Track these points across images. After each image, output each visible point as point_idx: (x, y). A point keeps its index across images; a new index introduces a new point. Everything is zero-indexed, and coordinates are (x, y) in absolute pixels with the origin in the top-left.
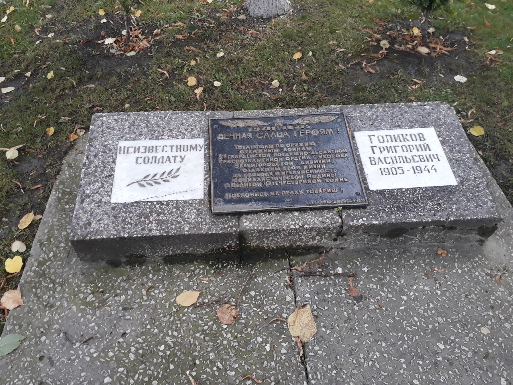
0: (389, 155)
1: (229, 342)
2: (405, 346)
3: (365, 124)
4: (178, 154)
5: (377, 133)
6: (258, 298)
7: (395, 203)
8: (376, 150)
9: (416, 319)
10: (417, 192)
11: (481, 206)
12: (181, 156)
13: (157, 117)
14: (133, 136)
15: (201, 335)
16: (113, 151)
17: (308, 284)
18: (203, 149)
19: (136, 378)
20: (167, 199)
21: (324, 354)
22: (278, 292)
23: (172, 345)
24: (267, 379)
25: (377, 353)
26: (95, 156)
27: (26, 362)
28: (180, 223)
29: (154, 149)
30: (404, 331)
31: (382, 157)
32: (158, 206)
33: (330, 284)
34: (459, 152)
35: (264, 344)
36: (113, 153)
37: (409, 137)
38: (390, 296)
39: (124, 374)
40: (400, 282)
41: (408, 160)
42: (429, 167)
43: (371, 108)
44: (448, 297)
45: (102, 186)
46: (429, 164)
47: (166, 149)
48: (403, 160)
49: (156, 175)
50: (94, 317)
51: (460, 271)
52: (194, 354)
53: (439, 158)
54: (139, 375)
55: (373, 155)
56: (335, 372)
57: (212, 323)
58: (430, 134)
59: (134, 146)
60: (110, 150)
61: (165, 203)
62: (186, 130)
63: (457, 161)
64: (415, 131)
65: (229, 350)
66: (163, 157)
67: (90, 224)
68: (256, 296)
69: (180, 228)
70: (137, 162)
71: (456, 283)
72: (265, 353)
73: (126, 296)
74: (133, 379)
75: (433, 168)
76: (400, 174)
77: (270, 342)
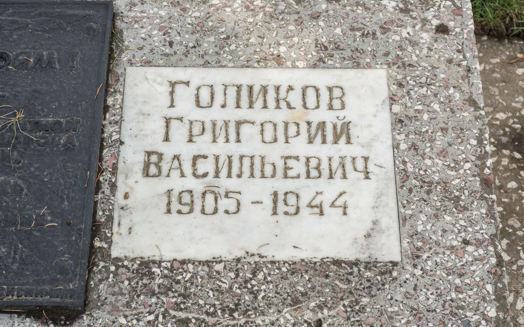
0: (211, 150)
3: (171, 44)
5: (198, 76)
7: (177, 307)
8: (179, 132)
10: (261, 276)
37: (295, 98)
41: (269, 170)
42: (327, 199)
46: (329, 190)
48: (263, 165)
53: (371, 167)
58: (367, 95)
63: (428, 186)
76: (227, 212)
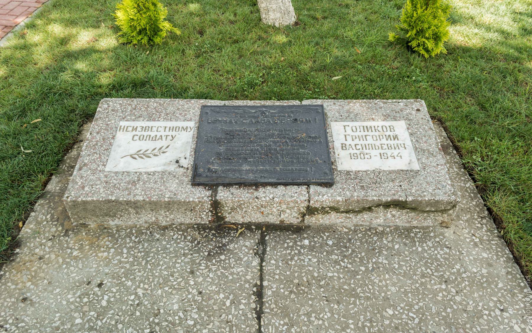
0: (360, 143)
1: (194, 296)
2: (356, 309)
4: (171, 133)
5: (351, 124)
6: (227, 261)
9: (370, 287)
11: (440, 189)
12: (172, 136)
13: (157, 103)
14: (134, 118)
15: (169, 289)
16: (114, 129)
17: (275, 252)
18: (193, 130)
19: (104, 321)
20: (153, 170)
21: (279, 311)
22: (246, 258)
23: (141, 295)
24: (223, 330)
25: (328, 314)
26: (98, 133)
27: (10, 302)
28: (163, 190)
29: (150, 129)
30: (357, 296)
31: (353, 144)
32: (145, 175)
33: (295, 253)
34: (426, 142)
35: (225, 300)
36: (114, 131)
37: (380, 129)
38: (349, 266)
39: (94, 317)
40: (361, 255)
42: (395, 154)
43: (349, 103)
44: (404, 270)
45: (100, 157)
46: (396, 152)
47: (160, 129)
49: (148, 150)
50: (77, 269)
51: (420, 249)
52: (160, 304)
53: (406, 146)
54: (108, 319)
55: (345, 142)
56: (286, 327)
57: (181, 279)
59: (132, 125)
60: (112, 129)
61: (152, 174)
62: (180, 114)
64: (387, 124)
65: (193, 303)
66: (156, 136)
67: (83, 188)
68: (225, 259)
69: (161, 195)
70: (133, 139)
71: (414, 259)
72: (224, 307)
73: (109, 253)
74: (101, 322)
75: (399, 155)
77: (231, 299)
